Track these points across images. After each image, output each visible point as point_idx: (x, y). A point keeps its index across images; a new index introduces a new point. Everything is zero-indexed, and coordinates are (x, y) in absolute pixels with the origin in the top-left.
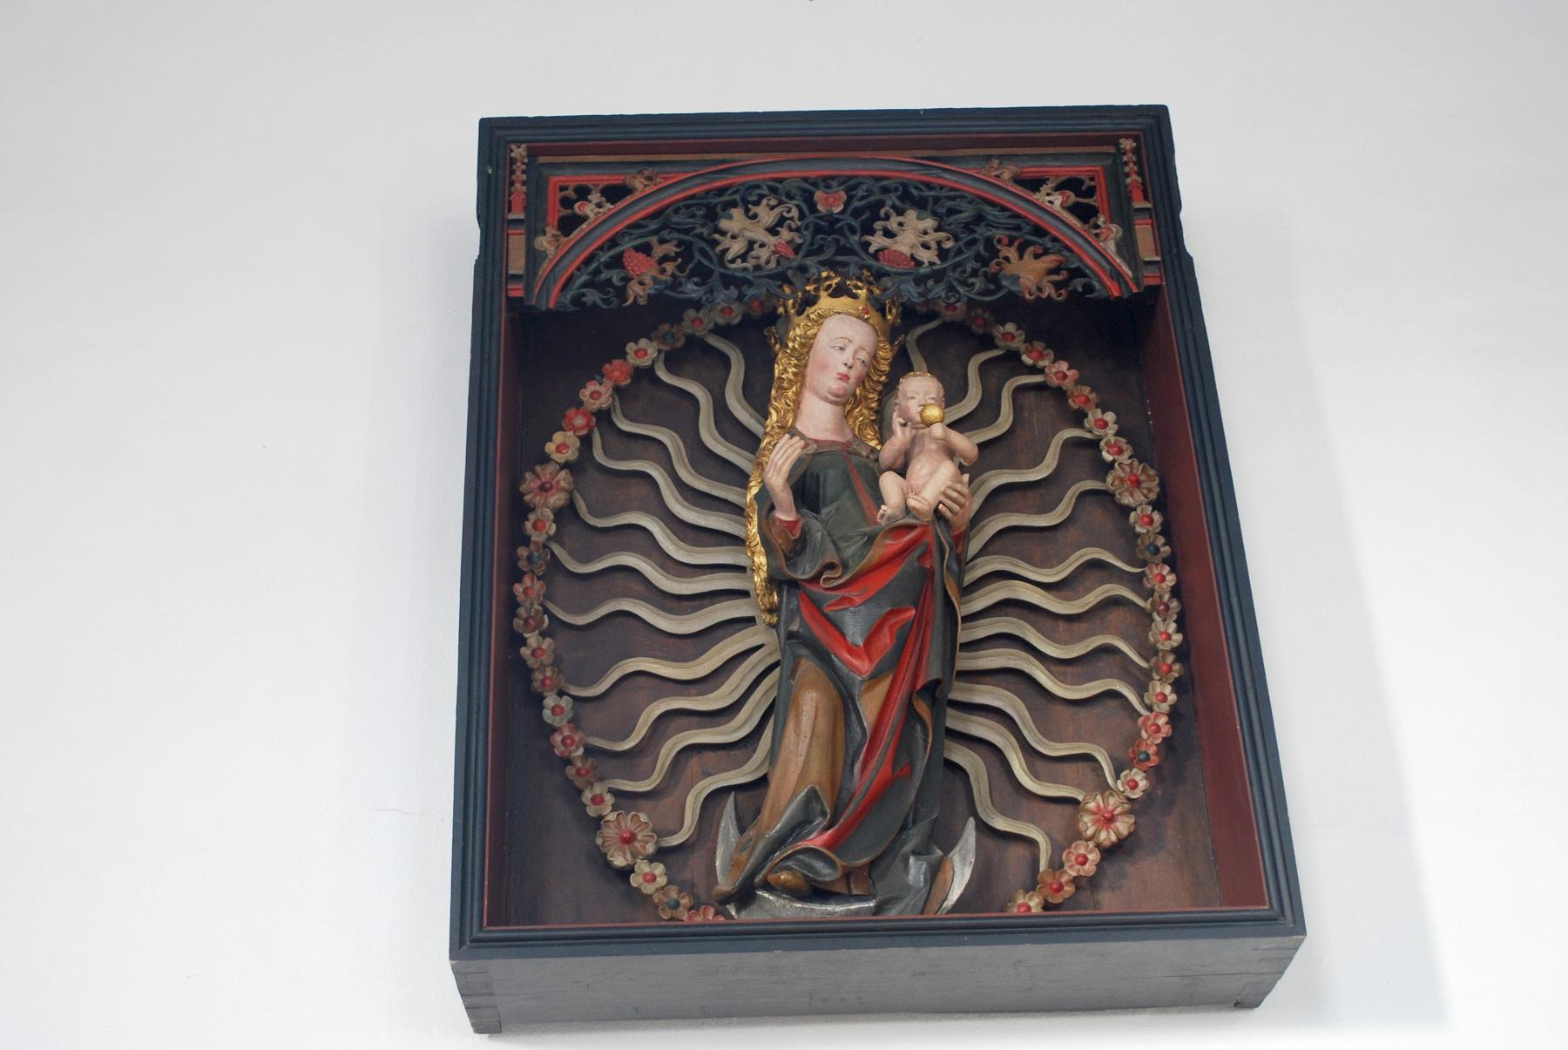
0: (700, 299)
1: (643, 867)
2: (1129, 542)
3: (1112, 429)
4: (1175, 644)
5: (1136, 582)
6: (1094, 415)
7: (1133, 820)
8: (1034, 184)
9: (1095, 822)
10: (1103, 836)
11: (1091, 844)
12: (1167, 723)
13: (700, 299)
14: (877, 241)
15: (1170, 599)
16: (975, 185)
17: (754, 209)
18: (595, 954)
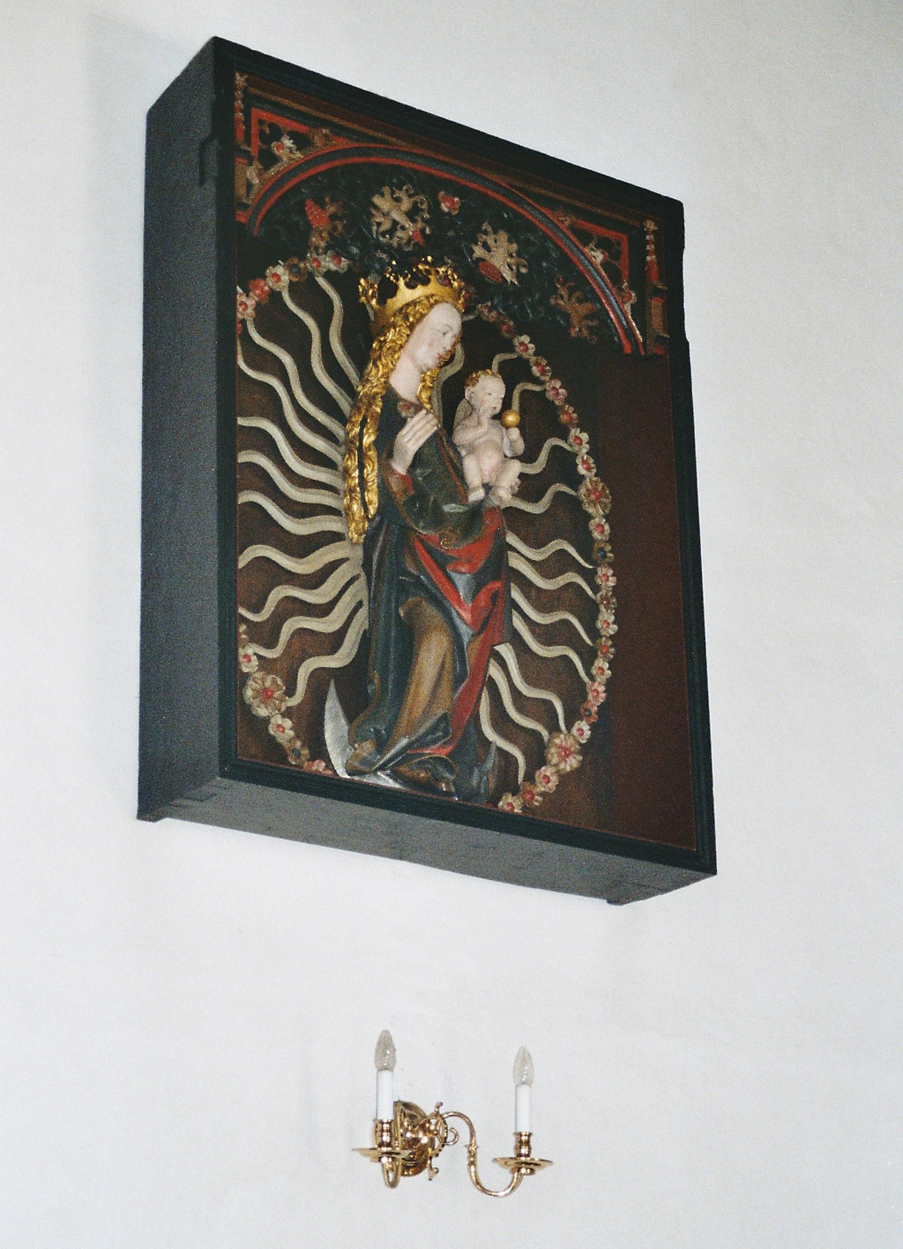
0: (551, 378)
1: (278, 720)
2: (585, 544)
3: (585, 448)
4: (612, 633)
5: (589, 576)
6: (575, 432)
7: (581, 758)
8: (585, 238)
9: (559, 754)
10: (562, 766)
11: (554, 770)
12: (605, 692)
13: (551, 378)
14: (479, 252)
15: (612, 596)
16: (452, 162)
17: (398, 194)
18: (399, 851)
